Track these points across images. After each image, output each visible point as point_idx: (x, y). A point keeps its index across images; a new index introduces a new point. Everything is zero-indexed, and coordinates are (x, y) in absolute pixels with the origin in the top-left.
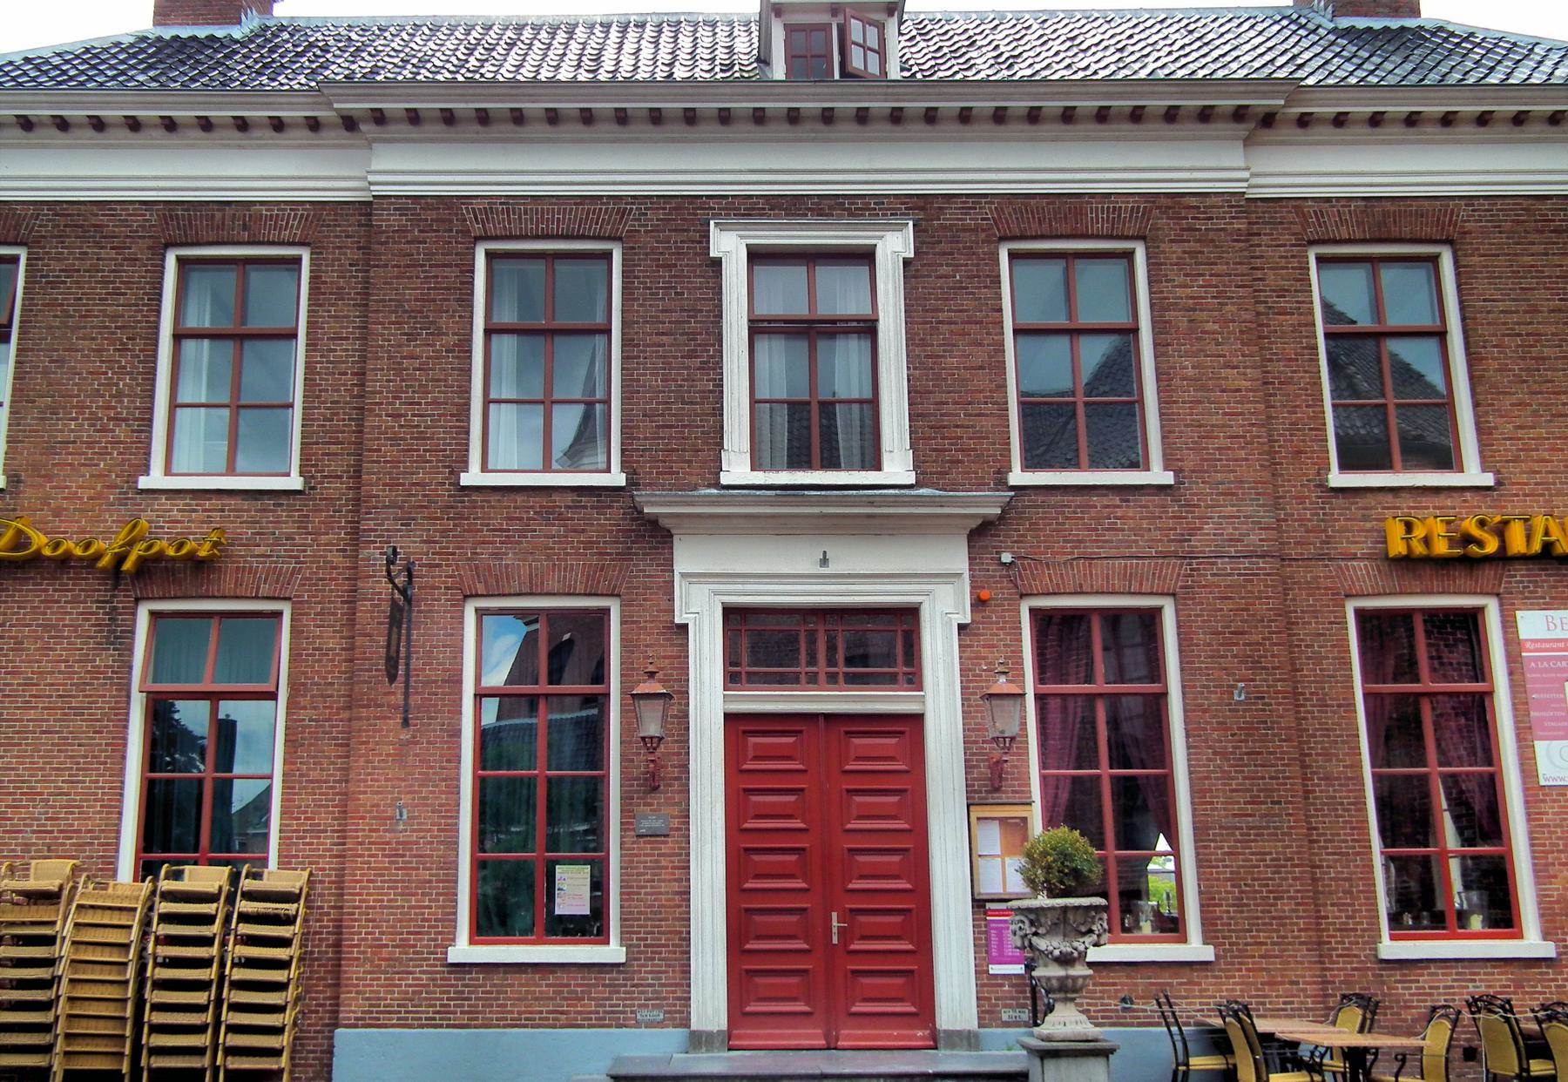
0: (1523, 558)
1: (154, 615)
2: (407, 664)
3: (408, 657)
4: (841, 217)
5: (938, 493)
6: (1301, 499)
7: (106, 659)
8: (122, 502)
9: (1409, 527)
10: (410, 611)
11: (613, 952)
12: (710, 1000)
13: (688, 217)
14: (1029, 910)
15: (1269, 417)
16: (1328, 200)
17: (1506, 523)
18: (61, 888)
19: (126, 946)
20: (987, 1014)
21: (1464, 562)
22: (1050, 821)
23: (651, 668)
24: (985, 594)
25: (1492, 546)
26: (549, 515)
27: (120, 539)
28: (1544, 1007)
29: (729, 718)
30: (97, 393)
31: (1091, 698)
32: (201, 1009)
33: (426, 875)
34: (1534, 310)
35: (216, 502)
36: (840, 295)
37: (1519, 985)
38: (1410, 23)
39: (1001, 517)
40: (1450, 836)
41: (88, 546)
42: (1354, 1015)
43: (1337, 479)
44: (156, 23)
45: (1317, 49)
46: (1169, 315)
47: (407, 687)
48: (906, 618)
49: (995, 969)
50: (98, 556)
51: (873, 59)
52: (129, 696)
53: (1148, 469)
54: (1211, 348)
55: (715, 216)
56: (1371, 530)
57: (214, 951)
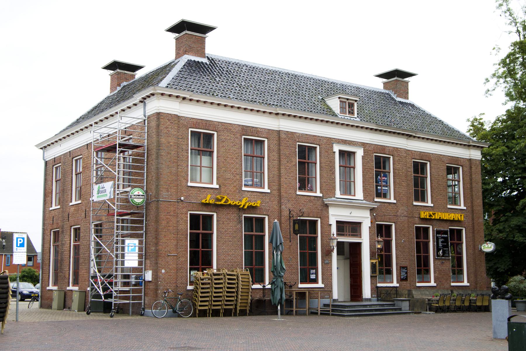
8: (239, 192)
26: (310, 201)
50: (240, 205)
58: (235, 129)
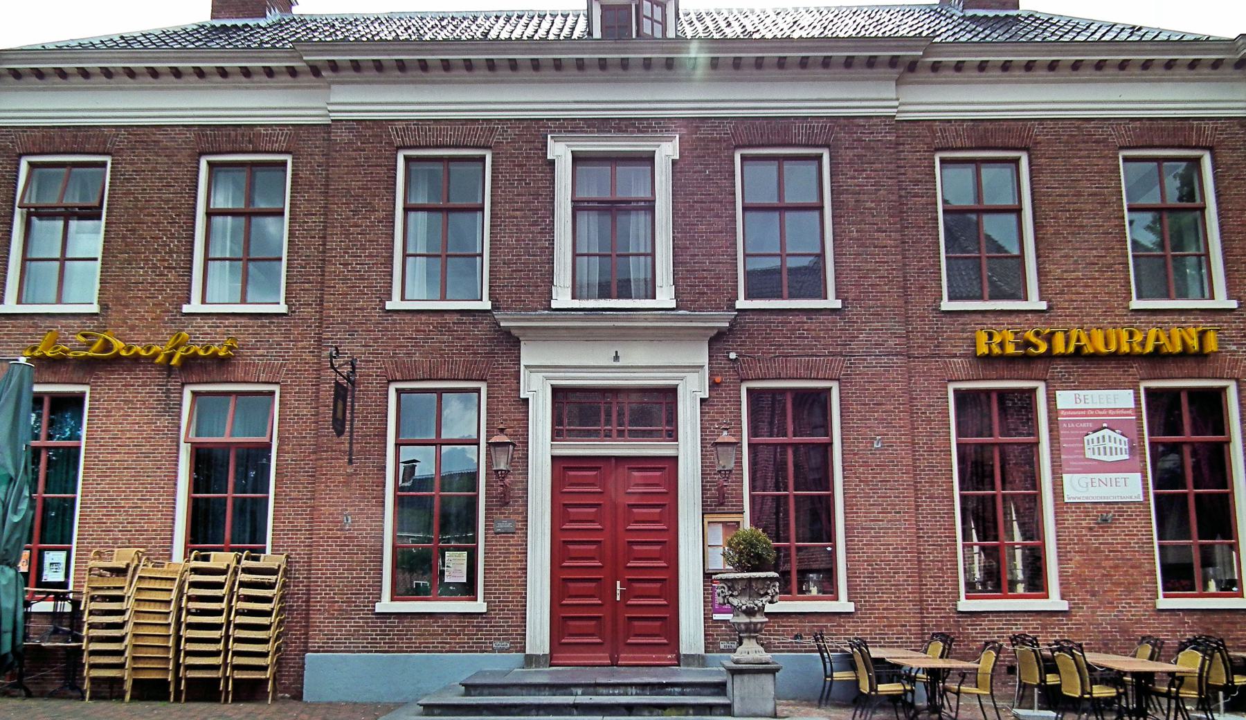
0: (1063, 357)
1: (195, 394)
2: (352, 425)
3: (352, 420)
4: (632, 132)
5: (1015, 524)
6: (922, 318)
7: (164, 422)
9: (991, 336)
10: (353, 391)
11: (479, 606)
12: (538, 636)
13: (535, 133)
14: (727, 580)
15: (905, 265)
16: (949, 121)
17: (1052, 334)
18: (128, 565)
19: (169, 602)
20: (710, 645)
21: (1025, 360)
22: (754, 522)
23: (501, 426)
24: (718, 379)
25: (1043, 348)
26: (442, 328)
27: (170, 344)
28: (1057, 642)
29: (554, 458)
30: (157, 251)
31: (784, 446)
32: (217, 641)
33: (362, 557)
34: (1078, 194)
35: (232, 321)
36: (630, 185)
37: (1044, 627)
38: (1013, 13)
39: (730, 329)
40: (1018, 538)
41: (149, 349)
42: (939, 646)
43: (946, 305)
44: (212, 18)
45: (950, 27)
46: (843, 197)
47: (351, 439)
48: (670, 394)
49: (717, 617)
50: (156, 355)
51: (658, 28)
52: (178, 446)
53: (826, 298)
54: (869, 219)
55: (551, 132)
56: (967, 338)
57: (224, 605)
58: (173, 139)
